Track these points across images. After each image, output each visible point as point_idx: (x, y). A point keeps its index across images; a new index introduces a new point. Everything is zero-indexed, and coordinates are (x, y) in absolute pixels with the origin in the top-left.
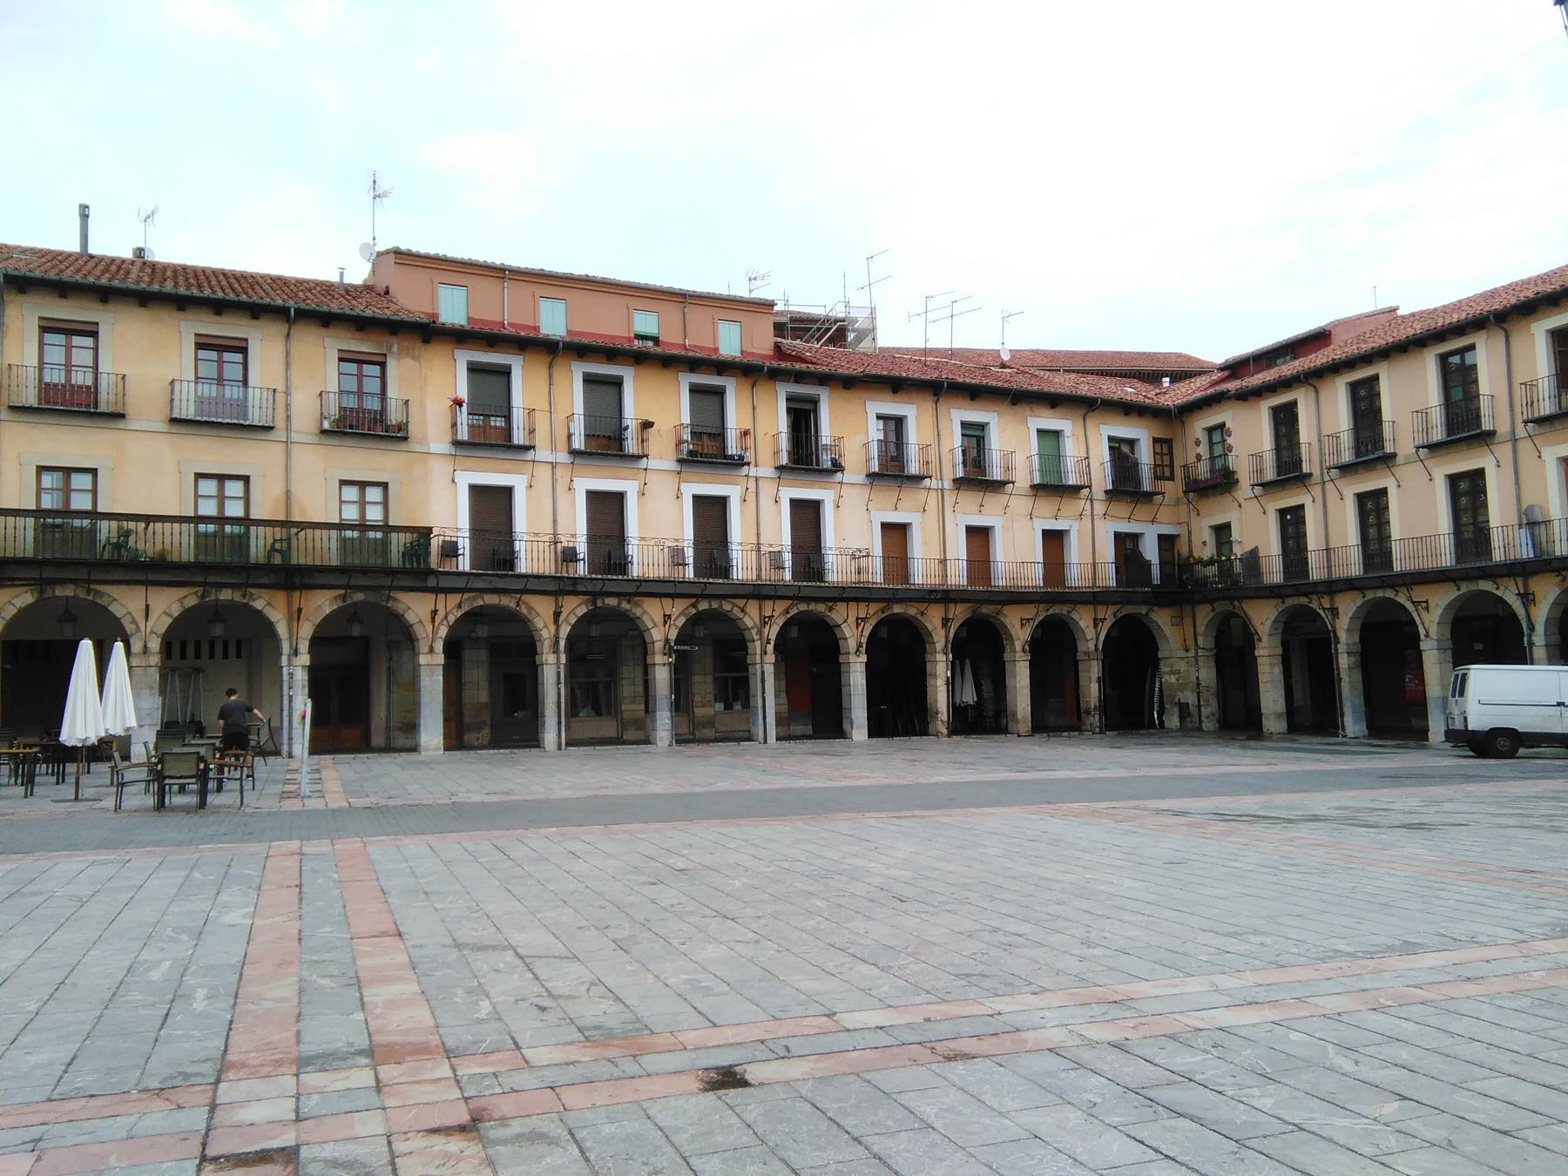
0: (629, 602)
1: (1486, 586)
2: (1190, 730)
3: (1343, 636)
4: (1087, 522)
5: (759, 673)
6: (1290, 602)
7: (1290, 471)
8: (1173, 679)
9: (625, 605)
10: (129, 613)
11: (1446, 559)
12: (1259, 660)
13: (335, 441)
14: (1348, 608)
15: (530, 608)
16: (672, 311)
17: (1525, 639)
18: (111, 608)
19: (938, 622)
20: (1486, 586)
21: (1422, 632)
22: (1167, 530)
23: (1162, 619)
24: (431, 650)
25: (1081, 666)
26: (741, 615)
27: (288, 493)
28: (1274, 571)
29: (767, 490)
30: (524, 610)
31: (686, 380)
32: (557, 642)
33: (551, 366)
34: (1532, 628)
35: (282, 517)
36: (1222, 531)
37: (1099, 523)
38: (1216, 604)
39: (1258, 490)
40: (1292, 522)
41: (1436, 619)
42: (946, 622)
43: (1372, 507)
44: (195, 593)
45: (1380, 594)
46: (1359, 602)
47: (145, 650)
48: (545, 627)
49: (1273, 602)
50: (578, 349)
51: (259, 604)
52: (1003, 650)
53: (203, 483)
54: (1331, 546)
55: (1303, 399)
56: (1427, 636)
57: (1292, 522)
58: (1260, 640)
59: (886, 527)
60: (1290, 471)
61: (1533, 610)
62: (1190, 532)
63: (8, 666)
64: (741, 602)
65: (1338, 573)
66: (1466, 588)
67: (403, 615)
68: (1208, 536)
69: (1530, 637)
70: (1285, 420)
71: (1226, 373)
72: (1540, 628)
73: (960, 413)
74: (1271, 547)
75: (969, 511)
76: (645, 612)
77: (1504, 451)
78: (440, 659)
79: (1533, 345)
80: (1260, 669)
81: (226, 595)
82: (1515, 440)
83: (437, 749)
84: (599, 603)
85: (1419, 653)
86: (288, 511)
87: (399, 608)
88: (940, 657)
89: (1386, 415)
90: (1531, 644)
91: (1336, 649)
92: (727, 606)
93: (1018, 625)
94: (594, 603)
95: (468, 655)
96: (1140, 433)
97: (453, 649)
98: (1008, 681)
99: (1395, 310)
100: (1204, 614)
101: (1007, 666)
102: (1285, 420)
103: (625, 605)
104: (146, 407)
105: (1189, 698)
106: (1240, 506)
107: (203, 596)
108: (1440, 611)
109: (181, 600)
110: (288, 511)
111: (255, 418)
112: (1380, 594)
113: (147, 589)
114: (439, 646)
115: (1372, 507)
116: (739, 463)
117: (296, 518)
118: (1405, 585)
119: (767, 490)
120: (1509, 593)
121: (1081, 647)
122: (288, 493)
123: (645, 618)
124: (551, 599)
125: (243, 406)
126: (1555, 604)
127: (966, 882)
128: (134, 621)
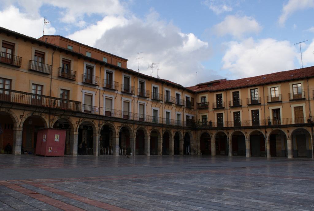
0: (112, 123)
1: (258, 130)
2: (196, 155)
3: (230, 138)
4: (183, 113)
5: (133, 140)
6: (219, 131)
7: (220, 106)
8: (193, 145)
9: (111, 123)
10: (17, 117)
11: (251, 125)
12: (212, 142)
13: (60, 79)
14: (231, 133)
15: (94, 123)
16: (110, 58)
17: (265, 139)
18: (13, 115)
19: (161, 131)
20: (258, 130)
21: (246, 137)
22: (193, 116)
23: (192, 132)
24: (76, 131)
25: (180, 142)
26: (130, 127)
27: (51, 90)
28: (215, 125)
29: (136, 100)
30: (93, 123)
31: (124, 74)
32: (99, 132)
33: (53, 54)
34: (266, 137)
35: (49, 96)
36: (204, 118)
37: (185, 113)
38: (202, 131)
39: (213, 110)
40: (220, 116)
41: (230, 136)
42: (163, 131)
43: (237, 115)
44: (31, 113)
45: (238, 130)
46: (217, 132)
47: (20, 126)
48: (97, 127)
49: (215, 131)
50: (107, 65)
51: (43, 117)
52: (169, 138)
53: (294, 86)
54: (229, 121)
55: (223, 94)
56: (247, 138)
57: (220, 116)
58: (212, 138)
59: (154, 110)
60: (220, 106)
61: (229, 135)
62: (197, 117)
63: (222, 122)
64: (131, 125)
65: (229, 126)
66: (254, 130)
67: (16, 123)
68: (201, 118)
69: (266, 139)
70: (219, 97)
71: (198, 87)
72: (230, 138)
73: (166, 89)
74: (215, 120)
75: (167, 109)
76: (115, 125)
77: (263, 107)
78: (77, 133)
79: (289, 87)
80: (212, 143)
81: (37, 114)
82: (227, 109)
83: (76, 155)
84: (107, 123)
85: (245, 141)
86: (50, 95)
87: (70, 120)
88: (162, 139)
89: (240, 98)
90: (266, 140)
91: (228, 140)
92: (128, 125)
93: (173, 133)
94: (106, 123)
95: (83, 132)
96: (189, 96)
97: (80, 131)
98: (170, 144)
99: (226, 79)
100: (199, 133)
101: (170, 141)
102: (219, 97)
103: (111, 123)
104: (25, 65)
105: (195, 149)
106: (209, 112)
107: (33, 114)
108: (214, 135)
109: (28, 114)
110: (50, 95)
111: (46, 71)
112: (238, 130)
113: (24, 112)
114: (77, 130)
115: (237, 115)
116: (131, 94)
117: (52, 96)
118: (244, 129)
119: (136, 100)
120: (225, 132)
121: (180, 138)
122: (51, 90)
123: (115, 127)
124: (98, 121)
125: (42, 67)
126: (215, 135)
127: (67, 191)
128: (17, 119)
